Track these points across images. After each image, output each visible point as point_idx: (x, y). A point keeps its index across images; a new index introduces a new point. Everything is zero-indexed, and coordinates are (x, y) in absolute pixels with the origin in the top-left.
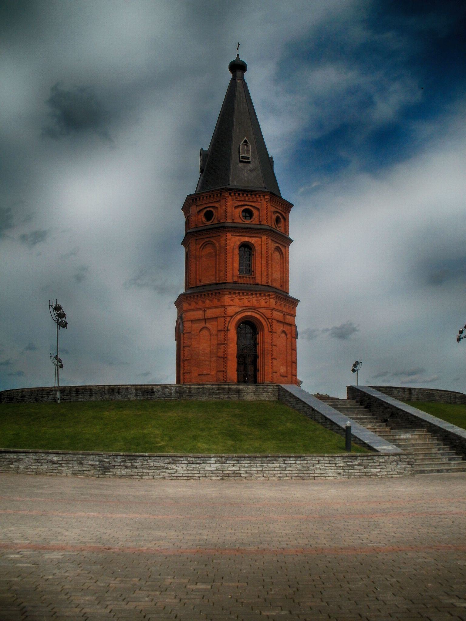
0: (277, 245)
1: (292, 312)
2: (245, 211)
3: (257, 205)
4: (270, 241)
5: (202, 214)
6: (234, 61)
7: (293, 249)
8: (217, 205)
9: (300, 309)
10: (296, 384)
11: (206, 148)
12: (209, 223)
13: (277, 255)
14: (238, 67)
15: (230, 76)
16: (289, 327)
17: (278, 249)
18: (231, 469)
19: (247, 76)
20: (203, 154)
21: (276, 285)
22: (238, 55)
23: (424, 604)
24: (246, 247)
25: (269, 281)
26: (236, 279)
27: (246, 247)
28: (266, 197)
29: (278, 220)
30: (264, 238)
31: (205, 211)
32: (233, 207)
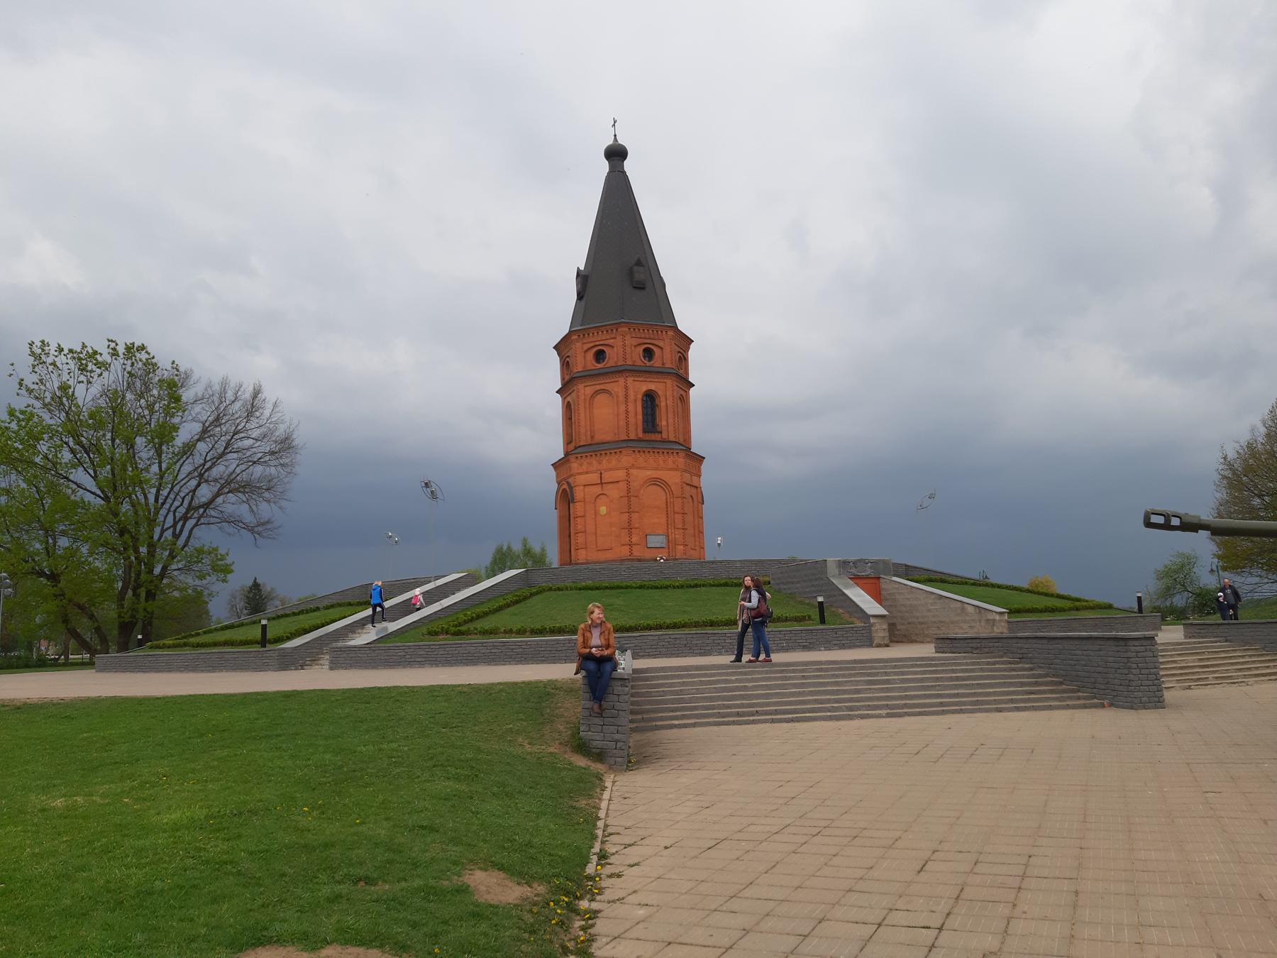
2: (645, 350)
3: (661, 344)
5: (590, 355)
8: (610, 342)
12: (599, 366)
14: (616, 154)
15: (604, 166)
19: (628, 165)
24: (650, 397)
26: (641, 435)
27: (650, 397)
30: (669, 382)
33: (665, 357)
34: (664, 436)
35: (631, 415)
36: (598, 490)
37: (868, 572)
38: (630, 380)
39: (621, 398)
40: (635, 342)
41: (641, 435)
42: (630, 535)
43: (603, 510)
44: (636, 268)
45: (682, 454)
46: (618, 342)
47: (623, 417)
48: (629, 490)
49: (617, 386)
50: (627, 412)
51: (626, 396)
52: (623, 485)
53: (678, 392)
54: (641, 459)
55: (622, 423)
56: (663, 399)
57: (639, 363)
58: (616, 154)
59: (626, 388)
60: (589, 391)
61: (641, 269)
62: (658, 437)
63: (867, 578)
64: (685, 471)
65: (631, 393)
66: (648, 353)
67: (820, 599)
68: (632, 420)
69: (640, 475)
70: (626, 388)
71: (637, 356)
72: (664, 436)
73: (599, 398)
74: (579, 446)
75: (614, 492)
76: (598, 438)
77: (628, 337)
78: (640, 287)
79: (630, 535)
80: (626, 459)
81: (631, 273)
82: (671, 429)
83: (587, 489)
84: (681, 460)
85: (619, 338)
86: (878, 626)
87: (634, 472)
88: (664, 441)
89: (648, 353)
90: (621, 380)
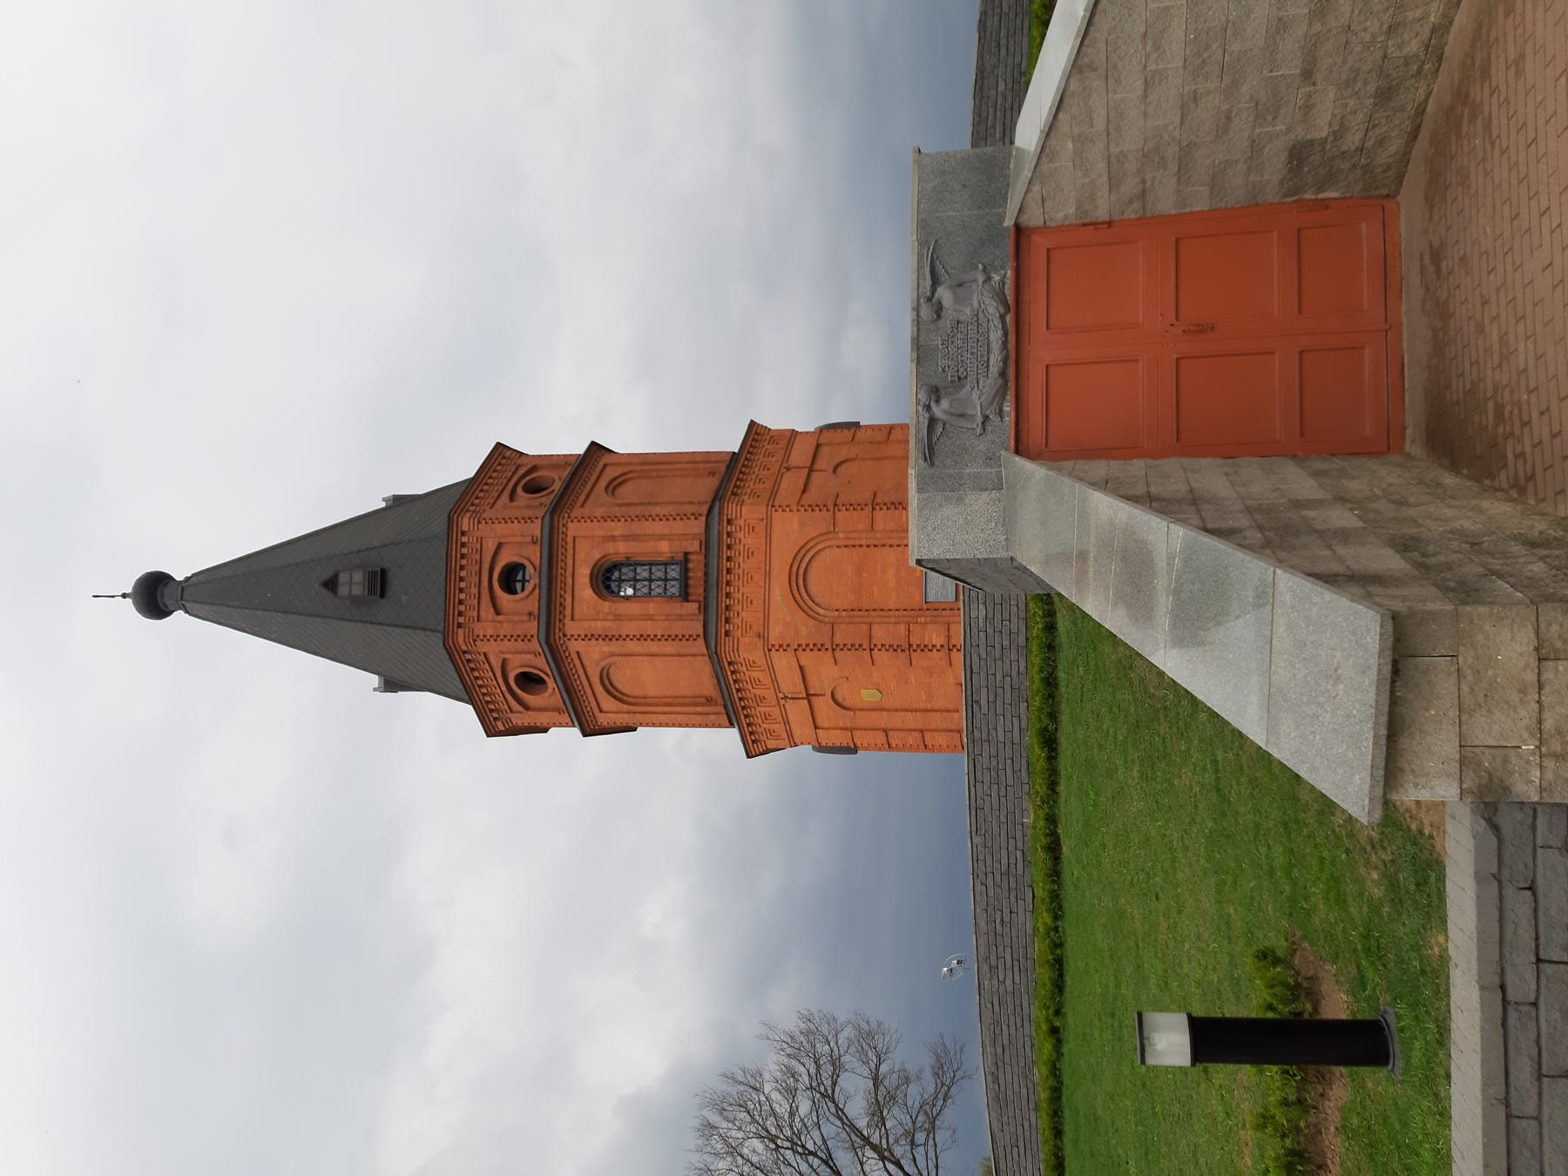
0: (602, 484)
1: (783, 444)
2: (511, 590)
3: (490, 546)
4: (586, 511)
5: (529, 699)
6: (135, 604)
7: (626, 440)
9: (774, 421)
10: (1467, 95)
11: (374, 680)
13: (628, 492)
14: (155, 595)
16: (824, 451)
17: (613, 486)
18: (1021, 918)
20: (391, 685)
21: (707, 486)
22: (124, 596)
23: (1555, 287)
24: (606, 578)
25: (692, 509)
26: (692, 607)
28: (465, 528)
29: (534, 488)
30: (574, 529)
31: (519, 692)
32: (500, 618)
33: (510, 533)
34: (693, 546)
35: (649, 628)
36: (823, 706)
37: (981, 303)
38: (571, 628)
39: (613, 647)
40: (487, 611)
41: (692, 607)
42: (924, 648)
43: (869, 696)
44: (343, 590)
45: (731, 510)
46: (491, 648)
47: (654, 647)
48: (820, 648)
49: (592, 655)
50: (641, 637)
51: (607, 638)
52: (807, 659)
53: (599, 503)
54: (745, 615)
55: (669, 648)
56: (611, 548)
57: (532, 604)
58: (155, 595)
59: (590, 637)
60: (608, 703)
61: (343, 577)
62: (696, 563)
63: (1016, 308)
64: (774, 493)
65: (598, 627)
66: (511, 578)
67: (1170, 1043)
68: (659, 628)
69: (784, 619)
70: (590, 637)
71: (521, 604)
72: (693, 546)
73: (621, 681)
74: (728, 704)
75: (824, 672)
76: (708, 687)
77: (479, 629)
78: (379, 582)
79: (924, 648)
80: (747, 650)
81: (354, 600)
82: (678, 527)
83: (820, 723)
84: (746, 512)
85: (483, 647)
86: (1505, 727)
87: (775, 635)
88: (706, 546)
89: (511, 578)
90: (574, 646)
